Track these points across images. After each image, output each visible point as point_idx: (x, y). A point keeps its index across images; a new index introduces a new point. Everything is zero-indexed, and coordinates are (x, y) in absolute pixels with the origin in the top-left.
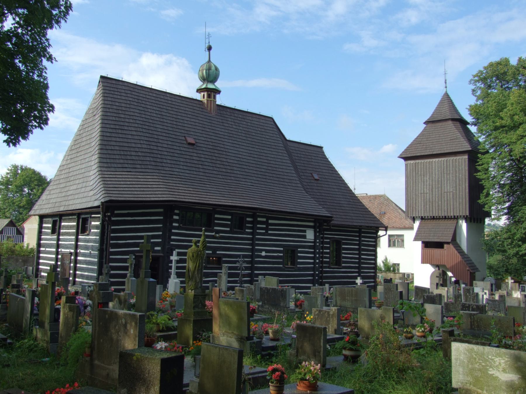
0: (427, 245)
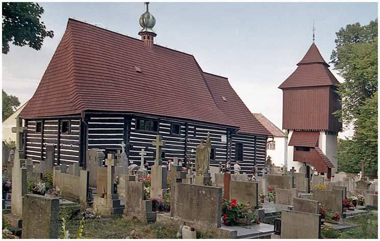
0: (297, 148)
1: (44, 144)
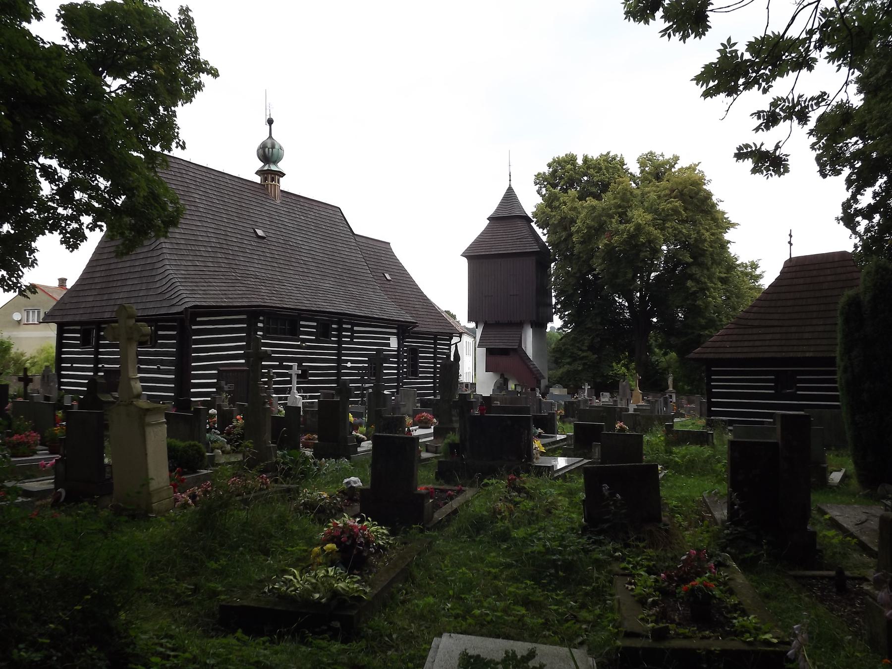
0: (490, 352)
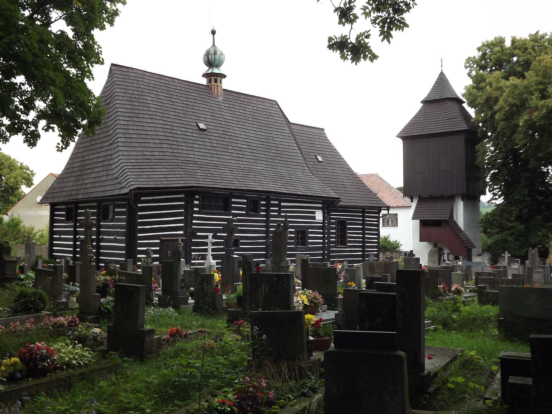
0: (424, 224)
1: (78, 237)
